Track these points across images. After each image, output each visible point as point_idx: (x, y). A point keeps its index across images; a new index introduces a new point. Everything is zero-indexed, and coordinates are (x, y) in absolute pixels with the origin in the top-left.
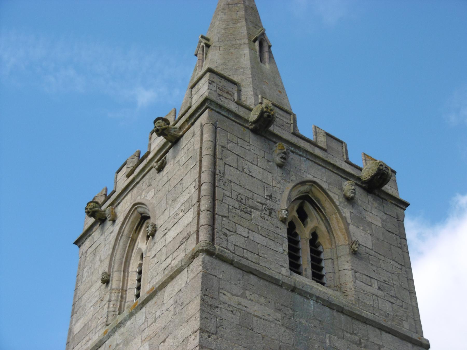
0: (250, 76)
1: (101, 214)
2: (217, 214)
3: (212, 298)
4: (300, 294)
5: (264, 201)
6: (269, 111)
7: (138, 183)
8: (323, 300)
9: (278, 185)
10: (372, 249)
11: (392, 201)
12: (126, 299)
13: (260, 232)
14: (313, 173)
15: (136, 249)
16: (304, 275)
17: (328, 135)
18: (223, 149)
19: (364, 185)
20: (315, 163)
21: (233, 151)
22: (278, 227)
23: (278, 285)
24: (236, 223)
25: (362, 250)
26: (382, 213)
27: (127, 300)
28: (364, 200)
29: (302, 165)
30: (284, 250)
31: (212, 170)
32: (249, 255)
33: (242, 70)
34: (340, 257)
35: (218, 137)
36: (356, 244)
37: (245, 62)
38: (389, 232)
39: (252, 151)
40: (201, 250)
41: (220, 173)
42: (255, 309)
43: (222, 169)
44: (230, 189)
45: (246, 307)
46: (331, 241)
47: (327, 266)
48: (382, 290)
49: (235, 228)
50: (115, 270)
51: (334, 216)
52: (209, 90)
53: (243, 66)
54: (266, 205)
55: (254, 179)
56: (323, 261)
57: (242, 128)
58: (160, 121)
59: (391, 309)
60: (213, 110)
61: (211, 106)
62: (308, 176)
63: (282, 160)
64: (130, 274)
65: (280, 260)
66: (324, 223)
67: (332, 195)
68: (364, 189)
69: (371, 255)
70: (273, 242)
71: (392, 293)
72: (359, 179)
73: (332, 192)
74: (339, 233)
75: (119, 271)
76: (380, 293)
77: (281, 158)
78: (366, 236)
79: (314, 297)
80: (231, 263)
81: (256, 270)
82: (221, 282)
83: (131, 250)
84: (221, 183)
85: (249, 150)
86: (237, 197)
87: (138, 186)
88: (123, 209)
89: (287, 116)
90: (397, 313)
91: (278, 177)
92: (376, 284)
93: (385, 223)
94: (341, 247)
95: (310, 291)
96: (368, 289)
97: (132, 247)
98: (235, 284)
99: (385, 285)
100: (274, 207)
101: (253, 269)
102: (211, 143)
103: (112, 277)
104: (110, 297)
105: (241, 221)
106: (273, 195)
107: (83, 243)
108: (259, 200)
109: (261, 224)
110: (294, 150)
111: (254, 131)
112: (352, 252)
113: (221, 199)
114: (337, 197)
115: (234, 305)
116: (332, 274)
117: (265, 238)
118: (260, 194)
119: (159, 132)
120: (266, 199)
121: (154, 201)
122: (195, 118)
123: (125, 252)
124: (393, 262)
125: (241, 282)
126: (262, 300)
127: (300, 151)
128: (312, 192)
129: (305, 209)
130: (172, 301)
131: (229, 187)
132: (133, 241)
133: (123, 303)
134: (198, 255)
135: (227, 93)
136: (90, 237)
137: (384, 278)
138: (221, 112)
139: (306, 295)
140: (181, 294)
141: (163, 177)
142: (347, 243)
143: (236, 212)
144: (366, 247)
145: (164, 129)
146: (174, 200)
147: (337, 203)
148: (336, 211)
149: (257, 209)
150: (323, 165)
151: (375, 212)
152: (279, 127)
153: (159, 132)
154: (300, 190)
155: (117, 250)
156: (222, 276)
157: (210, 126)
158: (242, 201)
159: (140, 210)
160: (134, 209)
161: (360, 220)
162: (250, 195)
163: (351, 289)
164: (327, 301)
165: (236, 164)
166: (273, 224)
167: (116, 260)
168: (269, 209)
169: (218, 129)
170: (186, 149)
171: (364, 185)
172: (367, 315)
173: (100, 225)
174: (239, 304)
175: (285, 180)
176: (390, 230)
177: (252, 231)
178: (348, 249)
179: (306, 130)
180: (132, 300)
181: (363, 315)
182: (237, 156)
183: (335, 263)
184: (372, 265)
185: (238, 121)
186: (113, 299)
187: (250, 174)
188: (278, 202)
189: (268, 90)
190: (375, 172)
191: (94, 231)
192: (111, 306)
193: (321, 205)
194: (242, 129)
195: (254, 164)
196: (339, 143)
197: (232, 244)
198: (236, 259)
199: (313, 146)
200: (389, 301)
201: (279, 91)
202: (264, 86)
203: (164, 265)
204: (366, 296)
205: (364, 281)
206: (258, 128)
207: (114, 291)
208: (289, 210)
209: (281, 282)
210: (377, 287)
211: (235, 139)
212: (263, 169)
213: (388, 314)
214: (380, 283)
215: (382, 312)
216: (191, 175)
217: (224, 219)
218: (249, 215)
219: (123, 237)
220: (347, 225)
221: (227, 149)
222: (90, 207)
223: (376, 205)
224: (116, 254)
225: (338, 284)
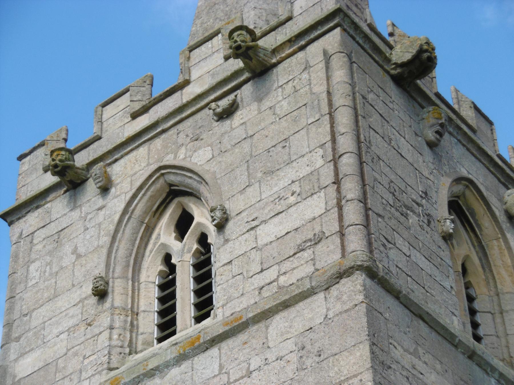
1: (76, 173)
3: (382, 350)
4: (479, 365)
7: (164, 131)
12: (138, 328)
15: (155, 244)
20: (468, 149)
21: (376, 107)
23: (453, 345)
27: (141, 330)
34: (507, 312)
40: (359, 266)
41: (365, 140)
45: (422, 374)
46: (488, 283)
50: (116, 275)
56: (478, 314)
62: (462, 169)
64: (142, 286)
66: (477, 252)
74: (503, 272)
75: (124, 277)
77: (437, 132)
79: (497, 373)
81: (428, 313)
82: (388, 325)
83: (143, 245)
87: (164, 136)
88: (131, 171)
97: (146, 240)
103: (113, 287)
104: (112, 320)
107: (19, 218)
111: (397, 80)
115: (408, 368)
116: (494, 338)
120: (421, 197)
121: (213, 167)
122: (307, 38)
123: (133, 246)
126: (438, 367)
130: (290, 345)
132: (149, 230)
133: (134, 335)
134: (352, 273)
135: (356, 5)
136: (40, 210)
140: (311, 335)
141: (232, 129)
145: (249, 48)
146: (270, 173)
148: (500, 236)
150: (478, 156)
157: (344, 57)
159: (172, 178)
160: (158, 175)
162: (403, 186)
167: (119, 259)
170: (289, 88)
173: (65, 192)
174: (414, 367)
180: (150, 331)
183: (498, 320)
185: (377, 58)
186: (117, 324)
191: (49, 202)
192: (115, 337)
193: (476, 221)
194: (382, 73)
197: (393, 261)
203: (259, 281)
207: (117, 312)
212: (412, 145)
216: (311, 135)
219: (132, 220)
222: (59, 157)
224: (118, 247)
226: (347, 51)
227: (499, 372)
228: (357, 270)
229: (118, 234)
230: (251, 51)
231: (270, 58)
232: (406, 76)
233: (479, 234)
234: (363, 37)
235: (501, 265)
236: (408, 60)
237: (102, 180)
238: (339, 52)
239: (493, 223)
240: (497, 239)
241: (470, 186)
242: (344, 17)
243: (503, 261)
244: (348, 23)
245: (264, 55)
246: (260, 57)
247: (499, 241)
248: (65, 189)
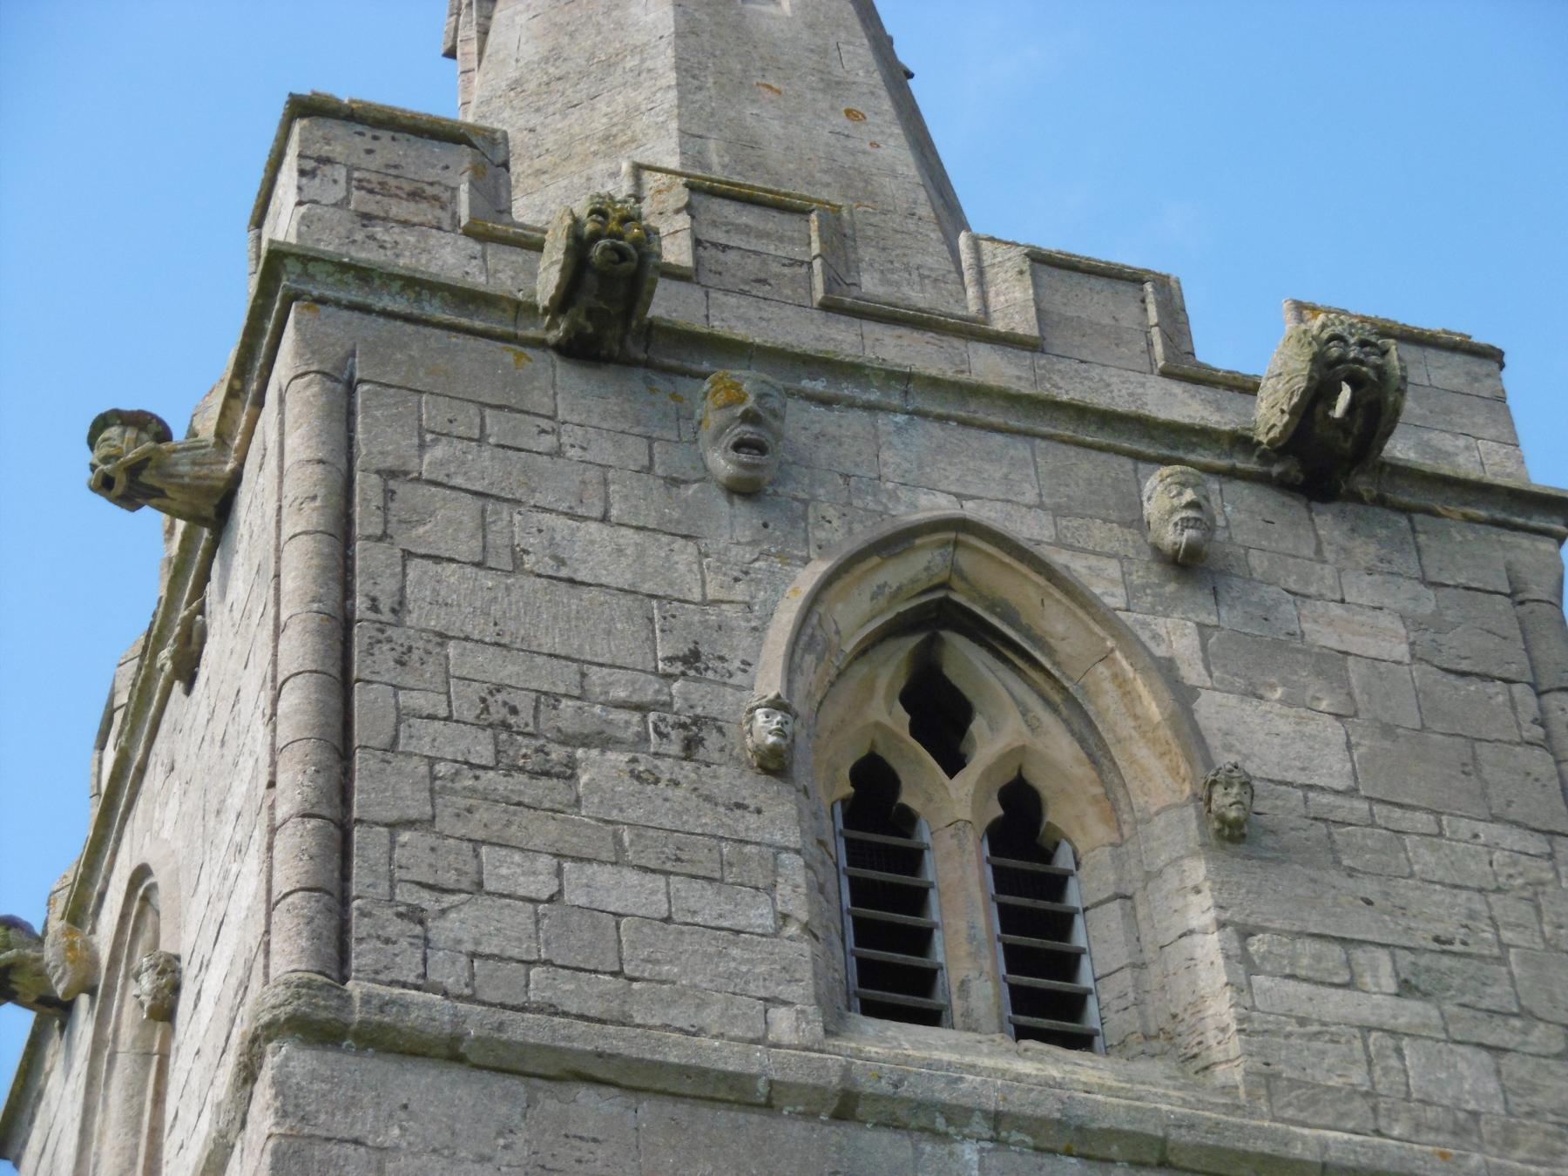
0: (671, 78)
2: (359, 821)
4: (891, 1124)
5: (650, 690)
6: (613, 226)
8: (1033, 1125)
9: (740, 592)
10: (1351, 792)
11: (1471, 511)
13: (630, 855)
14: (943, 479)
16: (957, 1019)
17: (1040, 260)
18: (392, 484)
19: (1276, 470)
20: (964, 423)
21: (458, 481)
22: (739, 806)
23: (751, 1106)
24: (476, 843)
25: (1272, 807)
26: (1410, 587)
28: (1287, 545)
29: (886, 455)
30: (785, 917)
31: (330, 605)
32: (565, 990)
33: (631, 63)
35: (360, 435)
36: (1228, 785)
37: (652, 16)
38: (1463, 674)
39: (571, 453)
41: (374, 608)
43: (386, 589)
44: (439, 679)
47: (1099, 941)
48: (1426, 996)
49: (471, 867)
51: (1102, 670)
52: (303, 209)
53: (639, 39)
54: (667, 706)
55: (586, 594)
56: (1079, 921)
57: (507, 355)
58: (113, 431)
59: (1492, 1086)
60: (322, 301)
61: (310, 287)
62: (924, 500)
63: (744, 457)
65: (762, 969)
67: (1077, 566)
68: (1283, 485)
69: (1344, 824)
70: (710, 891)
71: (1498, 995)
72: (1242, 442)
73: (1083, 550)
74: (1143, 753)
76: (1413, 1011)
77: (738, 447)
78: (1310, 728)
79: (977, 1117)
80: (450, 1052)
81: (600, 1055)
84: (385, 657)
85: (557, 453)
86: (486, 709)
89: (788, 224)
90: (1537, 1100)
91: (735, 550)
92: (1386, 967)
93: (1429, 636)
94: (1160, 822)
95: (945, 1097)
96: (1335, 1004)
98: (482, 1159)
99: (1446, 961)
100: (714, 710)
101: (585, 1053)
102: (319, 469)
105: (509, 824)
106: (704, 649)
108: (621, 694)
109: (633, 814)
110: (832, 391)
111: (580, 350)
112: (1219, 832)
113: (384, 739)
114: (1113, 569)
117: (660, 881)
118: (629, 661)
119: (118, 489)
120: (668, 677)
123: (136, 1132)
124: (1496, 829)
125: (519, 1139)
127: (867, 386)
128: (964, 578)
129: (951, 671)
131: (430, 668)
135: (415, 195)
137: (1439, 929)
138: (371, 300)
139: (923, 1122)
142: (1187, 789)
143: (480, 785)
144: (1311, 787)
145: (135, 469)
147: (1115, 599)
148: (1110, 643)
149: (603, 740)
151: (1361, 590)
152: (743, 292)
153: (118, 489)
154: (881, 588)
155: (101, 1134)
156: (396, 1131)
157: (309, 385)
158: (512, 720)
160: (136, 905)
161: (1265, 656)
162: (563, 679)
163: (1223, 1030)
164: (1060, 1124)
165: (476, 544)
166: (707, 798)
168: (683, 726)
169: (362, 389)
171: (1276, 470)
172: (1325, 1146)
175: (778, 555)
176: (1464, 666)
177: (575, 859)
178: (1194, 825)
181: (1297, 1151)
182: (479, 502)
184: (1351, 872)
185: (478, 324)
187: (564, 573)
188: (739, 679)
189: (776, 127)
190: (1301, 384)
195: (585, 518)
196: (1121, 286)
198: (476, 1022)
199: (957, 343)
200: (1480, 1045)
201: (848, 112)
202: (751, 109)
204: (1317, 1045)
205: (1302, 973)
206: (590, 330)
208: (798, 704)
209: (761, 1086)
210: (1390, 985)
211: (467, 420)
213: (1474, 1114)
214: (1411, 957)
215: (1430, 1114)
217: (405, 836)
218: (560, 784)
220: (1183, 696)
221: (418, 479)
223: (1365, 551)
224: (97, 1155)
225: (1163, 1020)
226: (321, 362)
227: (985, 1113)
228: (269, 1040)
229: (94, 1115)
230: (145, 473)
231: (219, 462)
232: (590, 330)
233: (1048, 666)
234: (403, 288)
235: (1133, 733)
236: (558, 287)
237: (64, 973)
238: (296, 377)
239: (1080, 613)
240: (1106, 657)
241: (962, 537)
242: (305, 265)
243: (1136, 717)
244: (329, 275)
245: (194, 463)
246: (182, 477)
247: (1114, 660)
248: (57, 1023)
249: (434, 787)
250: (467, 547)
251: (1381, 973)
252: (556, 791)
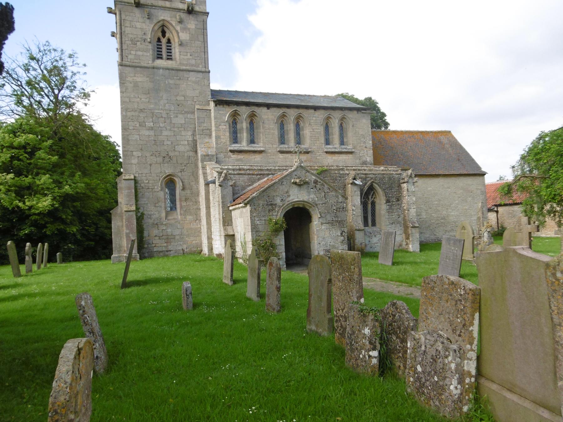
42: (139, 79)
67: (172, 22)
76: (191, 57)
96: (186, 57)
149: (138, 41)
151: (192, 22)
161: (185, 29)
162: (135, 36)
179: (513, 179)
220: (178, 33)
223: (193, 18)
249: (128, 46)
250: (129, 26)
251: (189, 54)
252: (135, 46)
